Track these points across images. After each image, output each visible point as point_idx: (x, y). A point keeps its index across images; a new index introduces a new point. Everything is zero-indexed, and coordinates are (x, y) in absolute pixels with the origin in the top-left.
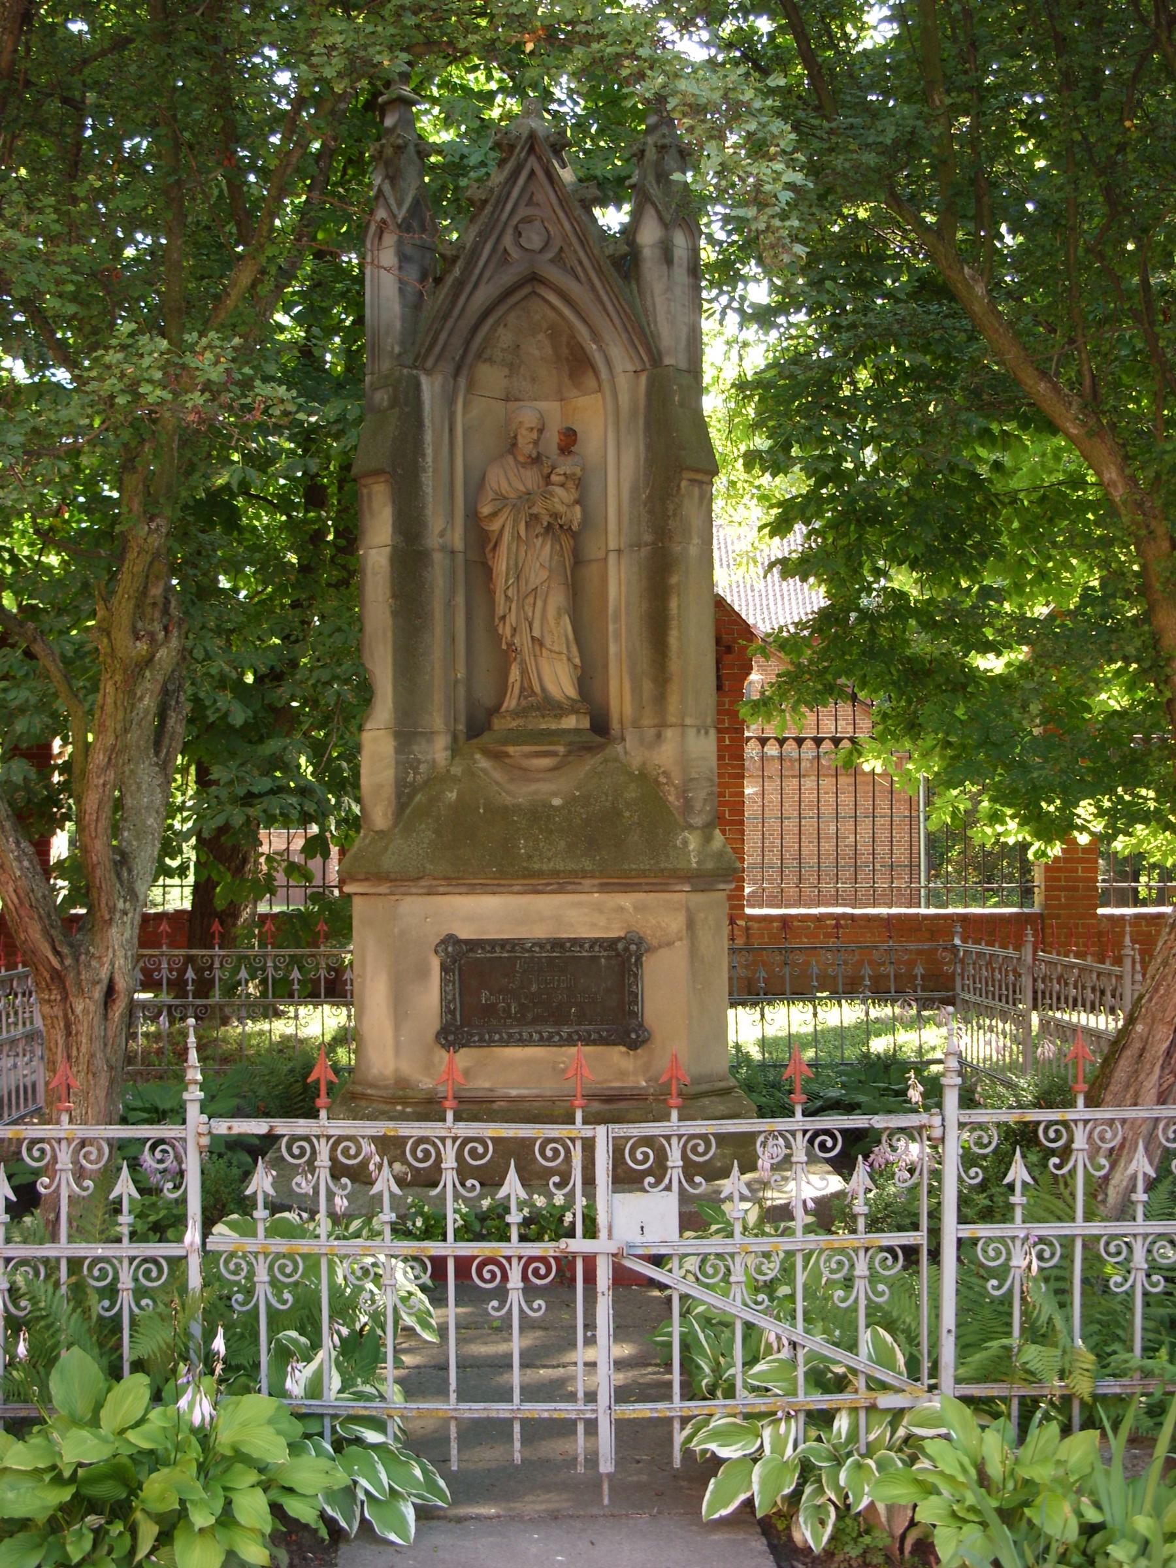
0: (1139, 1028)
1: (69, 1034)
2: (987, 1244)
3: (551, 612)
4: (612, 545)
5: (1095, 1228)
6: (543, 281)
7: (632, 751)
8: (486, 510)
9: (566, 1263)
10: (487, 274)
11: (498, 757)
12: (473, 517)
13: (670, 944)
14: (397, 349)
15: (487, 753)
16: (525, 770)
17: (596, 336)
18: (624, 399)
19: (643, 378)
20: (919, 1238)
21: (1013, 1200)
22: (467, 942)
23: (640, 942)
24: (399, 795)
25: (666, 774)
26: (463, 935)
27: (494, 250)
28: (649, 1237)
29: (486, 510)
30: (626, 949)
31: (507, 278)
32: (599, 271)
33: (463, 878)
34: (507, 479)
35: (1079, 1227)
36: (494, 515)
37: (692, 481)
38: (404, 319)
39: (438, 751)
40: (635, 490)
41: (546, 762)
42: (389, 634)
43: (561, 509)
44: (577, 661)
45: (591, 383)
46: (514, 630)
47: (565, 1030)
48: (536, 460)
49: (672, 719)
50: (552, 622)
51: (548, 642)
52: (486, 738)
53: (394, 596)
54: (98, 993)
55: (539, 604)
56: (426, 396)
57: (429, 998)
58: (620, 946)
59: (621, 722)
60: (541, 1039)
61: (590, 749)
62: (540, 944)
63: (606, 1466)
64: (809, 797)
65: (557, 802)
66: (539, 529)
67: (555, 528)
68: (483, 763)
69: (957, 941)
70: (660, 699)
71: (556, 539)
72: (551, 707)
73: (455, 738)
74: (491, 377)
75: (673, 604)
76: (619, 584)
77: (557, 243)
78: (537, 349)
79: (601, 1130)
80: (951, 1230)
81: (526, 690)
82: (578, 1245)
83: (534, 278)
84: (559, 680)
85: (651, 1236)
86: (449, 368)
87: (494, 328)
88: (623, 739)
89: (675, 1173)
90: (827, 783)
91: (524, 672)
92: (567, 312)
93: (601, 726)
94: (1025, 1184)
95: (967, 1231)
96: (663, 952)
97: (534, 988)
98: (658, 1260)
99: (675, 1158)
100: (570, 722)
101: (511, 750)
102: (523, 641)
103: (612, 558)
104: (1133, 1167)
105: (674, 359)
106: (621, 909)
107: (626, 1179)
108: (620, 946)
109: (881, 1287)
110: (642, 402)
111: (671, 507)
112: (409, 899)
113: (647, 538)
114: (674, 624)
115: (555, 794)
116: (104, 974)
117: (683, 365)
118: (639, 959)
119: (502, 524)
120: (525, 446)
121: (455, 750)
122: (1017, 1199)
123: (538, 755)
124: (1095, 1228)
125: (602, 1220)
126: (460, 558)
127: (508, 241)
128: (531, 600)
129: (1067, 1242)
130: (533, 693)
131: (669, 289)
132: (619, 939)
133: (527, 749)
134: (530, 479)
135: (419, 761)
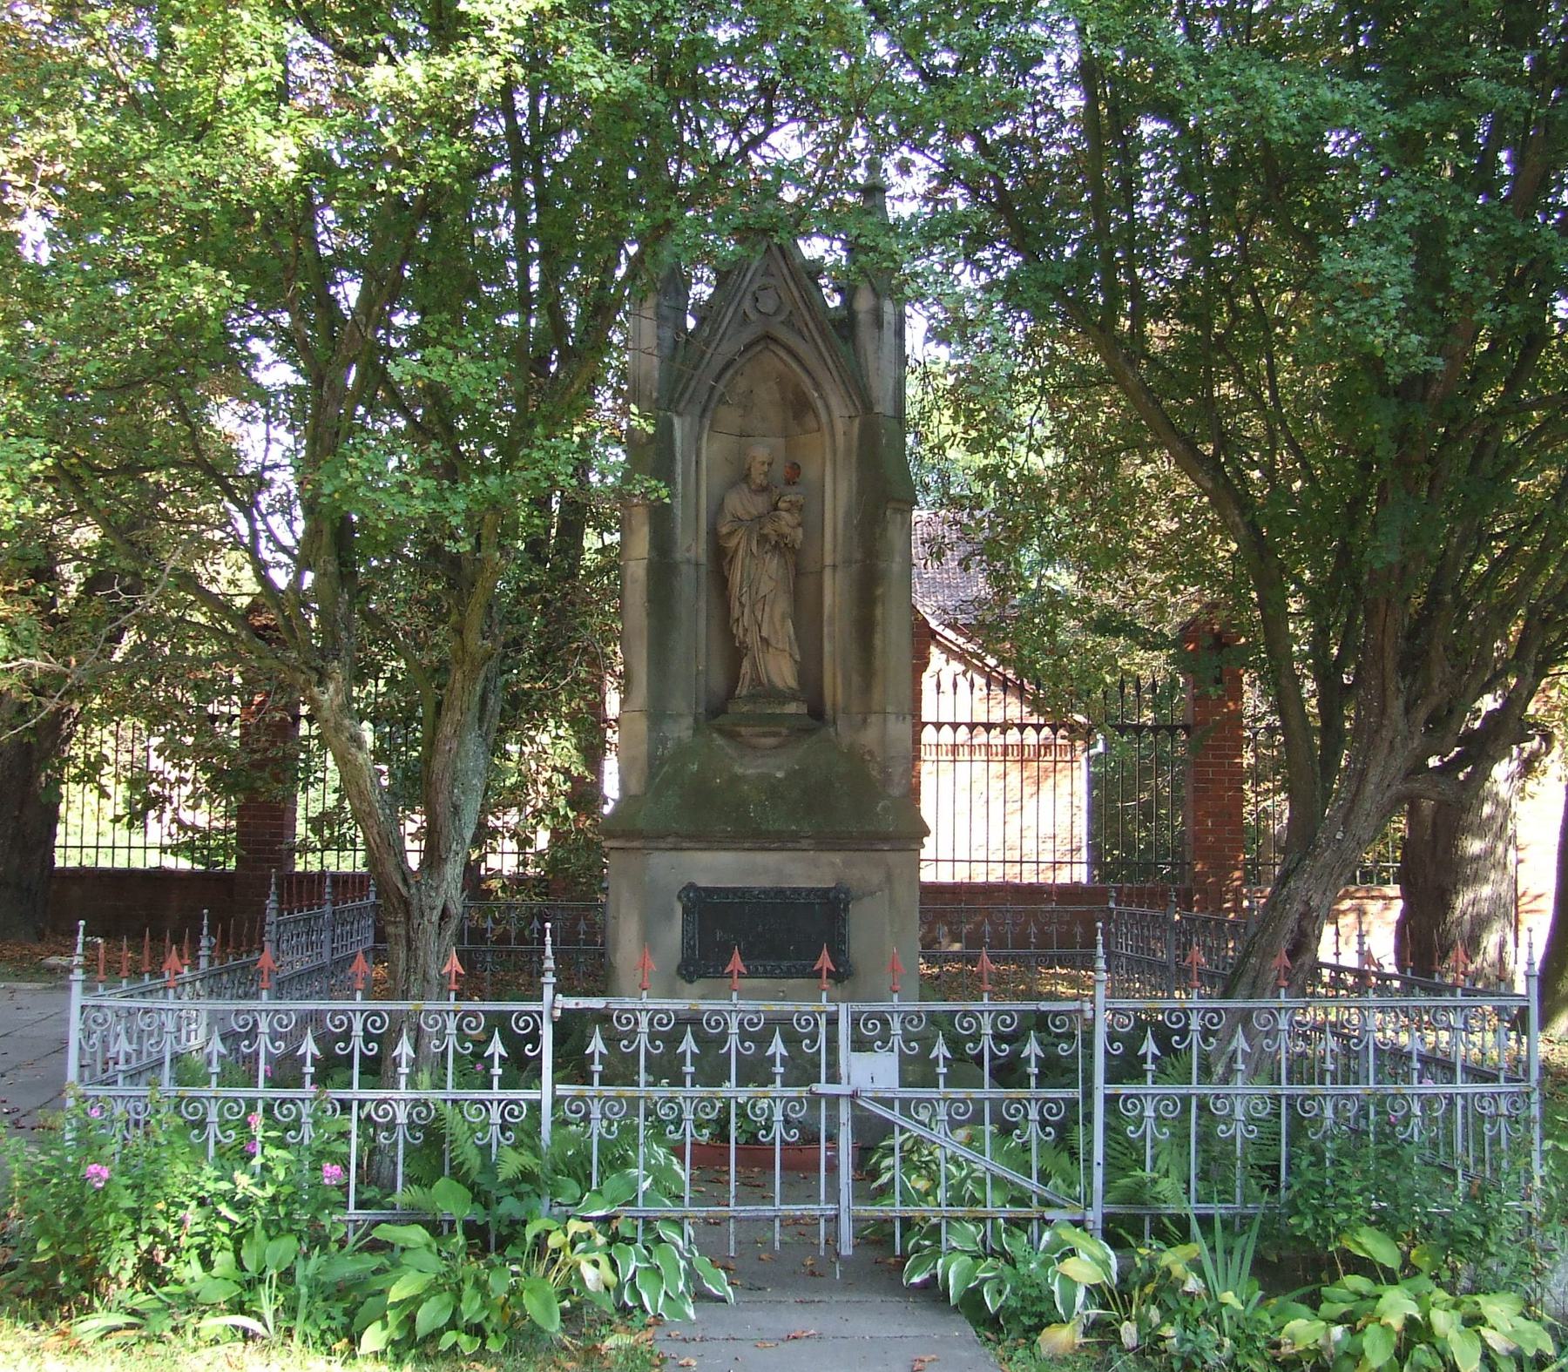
0: (1253, 960)
1: (409, 949)
2: (1125, 1101)
3: (777, 617)
4: (828, 560)
5: (1206, 1090)
6: (775, 340)
7: (843, 733)
8: (724, 530)
9: (815, 1099)
10: (730, 332)
11: (731, 735)
12: (713, 532)
13: (872, 894)
14: (655, 395)
15: (721, 731)
16: (754, 748)
17: (817, 386)
18: (840, 439)
19: (857, 422)
20: (1077, 1093)
21: (1146, 1067)
22: (705, 889)
23: (847, 892)
24: (650, 766)
25: (870, 752)
26: (702, 883)
27: (736, 311)
28: (877, 1085)
29: (724, 530)
30: (837, 898)
31: (747, 336)
32: (822, 332)
33: (704, 839)
34: (741, 503)
35: (1195, 1088)
36: (731, 534)
37: (896, 510)
38: (661, 370)
39: (681, 730)
40: (848, 514)
41: (771, 741)
42: (645, 633)
43: (787, 530)
44: (798, 657)
45: (811, 422)
46: (746, 630)
47: (785, 964)
48: (763, 489)
49: (876, 707)
50: (778, 627)
51: (773, 642)
52: (721, 720)
53: (649, 601)
54: (435, 917)
55: (767, 609)
56: (678, 434)
57: (673, 935)
58: (831, 895)
59: (835, 711)
60: (765, 972)
61: (809, 731)
62: (765, 891)
63: (846, 1250)
64: (963, 781)
65: (780, 775)
66: (768, 547)
67: (782, 547)
68: (719, 740)
69: (1112, 905)
70: (867, 688)
71: (782, 555)
72: (781, 697)
73: (696, 720)
74: (730, 416)
75: (879, 612)
76: (834, 592)
77: (788, 307)
78: (767, 394)
79: (843, 1007)
80: (1101, 1089)
81: (756, 680)
82: (822, 1087)
83: (768, 338)
84: (781, 670)
85: (880, 1084)
86: (698, 410)
87: (733, 377)
88: (835, 723)
89: (896, 1041)
90: (996, 768)
91: (754, 665)
92: (794, 365)
93: (817, 712)
94: (1155, 1057)
95: (1113, 1089)
96: (866, 900)
97: (760, 928)
98: (888, 1103)
99: (896, 1027)
100: (792, 708)
101: (743, 730)
102: (752, 639)
103: (828, 573)
104: (1234, 1043)
105: (885, 407)
106: (833, 864)
107: (860, 1044)
108: (831, 895)
109: (1048, 1129)
110: (855, 443)
111: (878, 531)
112: (657, 853)
113: (858, 556)
114: (879, 629)
115: (779, 769)
116: (439, 903)
117: (890, 412)
118: (846, 909)
119: (739, 543)
120: (758, 478)
121: (696, 730)
122: (1149, 1066)
123: (765, 735)
124: (1206, 1090)
125: (843, 1070)
126: (703, 570)
127: (747, 305)
128: (760, 605)
129: (1186, 1099)
130: (761, 684)
131: (879, 349)
132: (829, 889)
133: (757, 729)
134: (760, 504)
135: (667, 739)
